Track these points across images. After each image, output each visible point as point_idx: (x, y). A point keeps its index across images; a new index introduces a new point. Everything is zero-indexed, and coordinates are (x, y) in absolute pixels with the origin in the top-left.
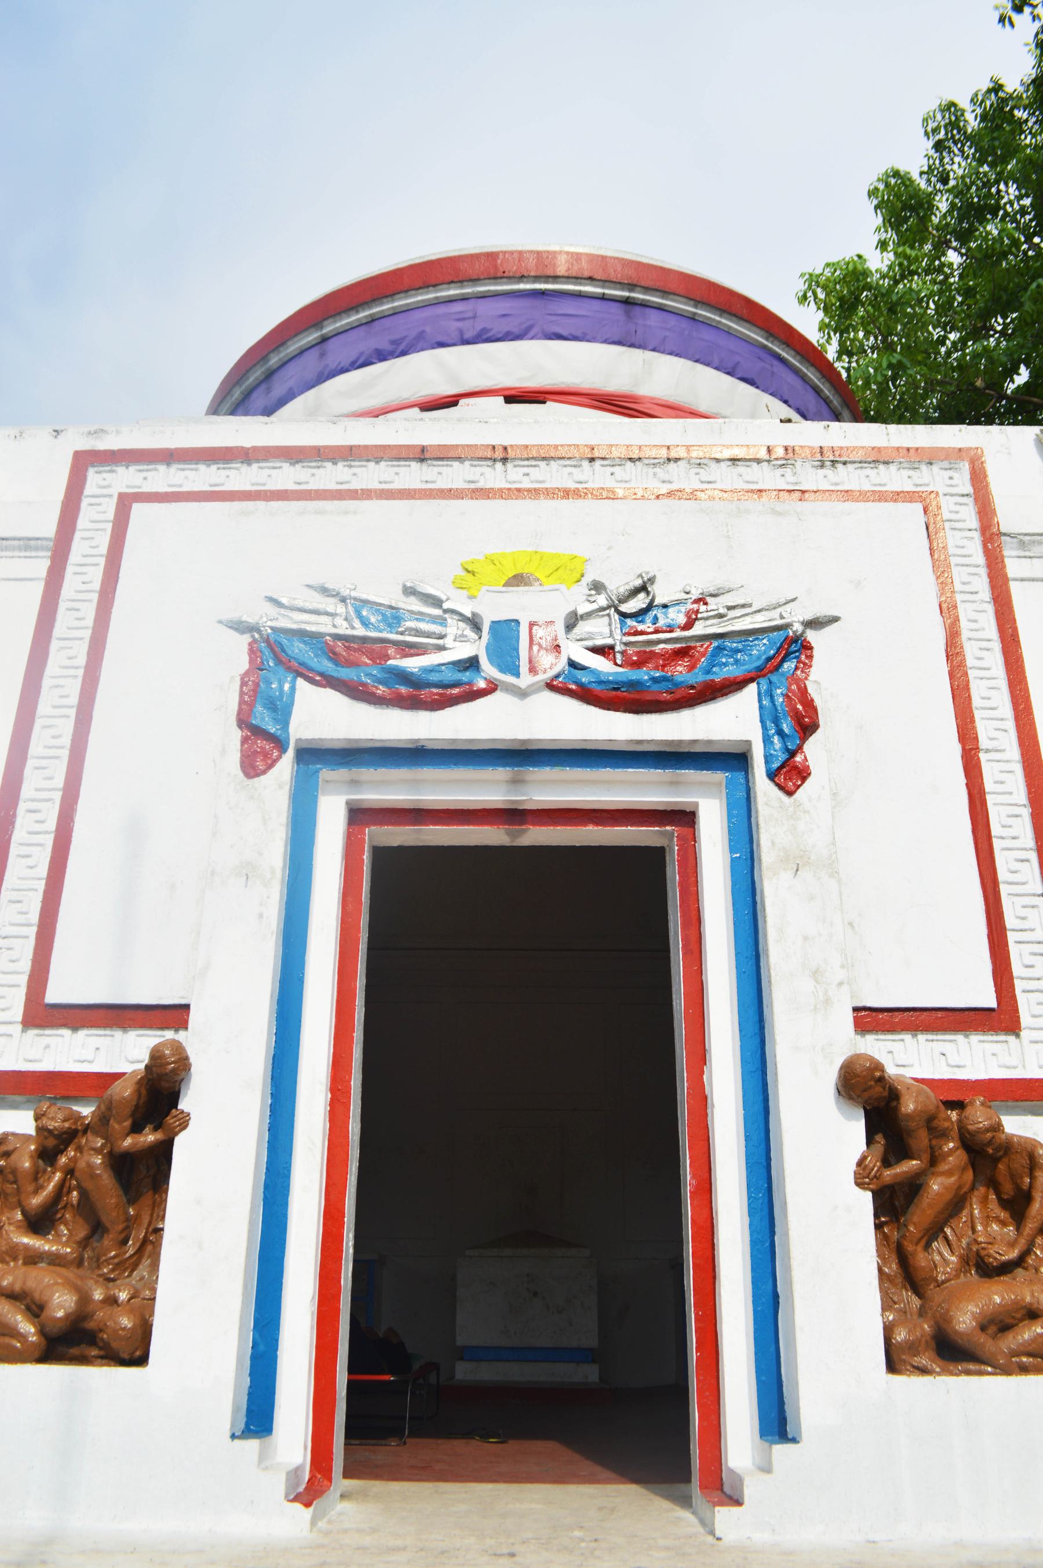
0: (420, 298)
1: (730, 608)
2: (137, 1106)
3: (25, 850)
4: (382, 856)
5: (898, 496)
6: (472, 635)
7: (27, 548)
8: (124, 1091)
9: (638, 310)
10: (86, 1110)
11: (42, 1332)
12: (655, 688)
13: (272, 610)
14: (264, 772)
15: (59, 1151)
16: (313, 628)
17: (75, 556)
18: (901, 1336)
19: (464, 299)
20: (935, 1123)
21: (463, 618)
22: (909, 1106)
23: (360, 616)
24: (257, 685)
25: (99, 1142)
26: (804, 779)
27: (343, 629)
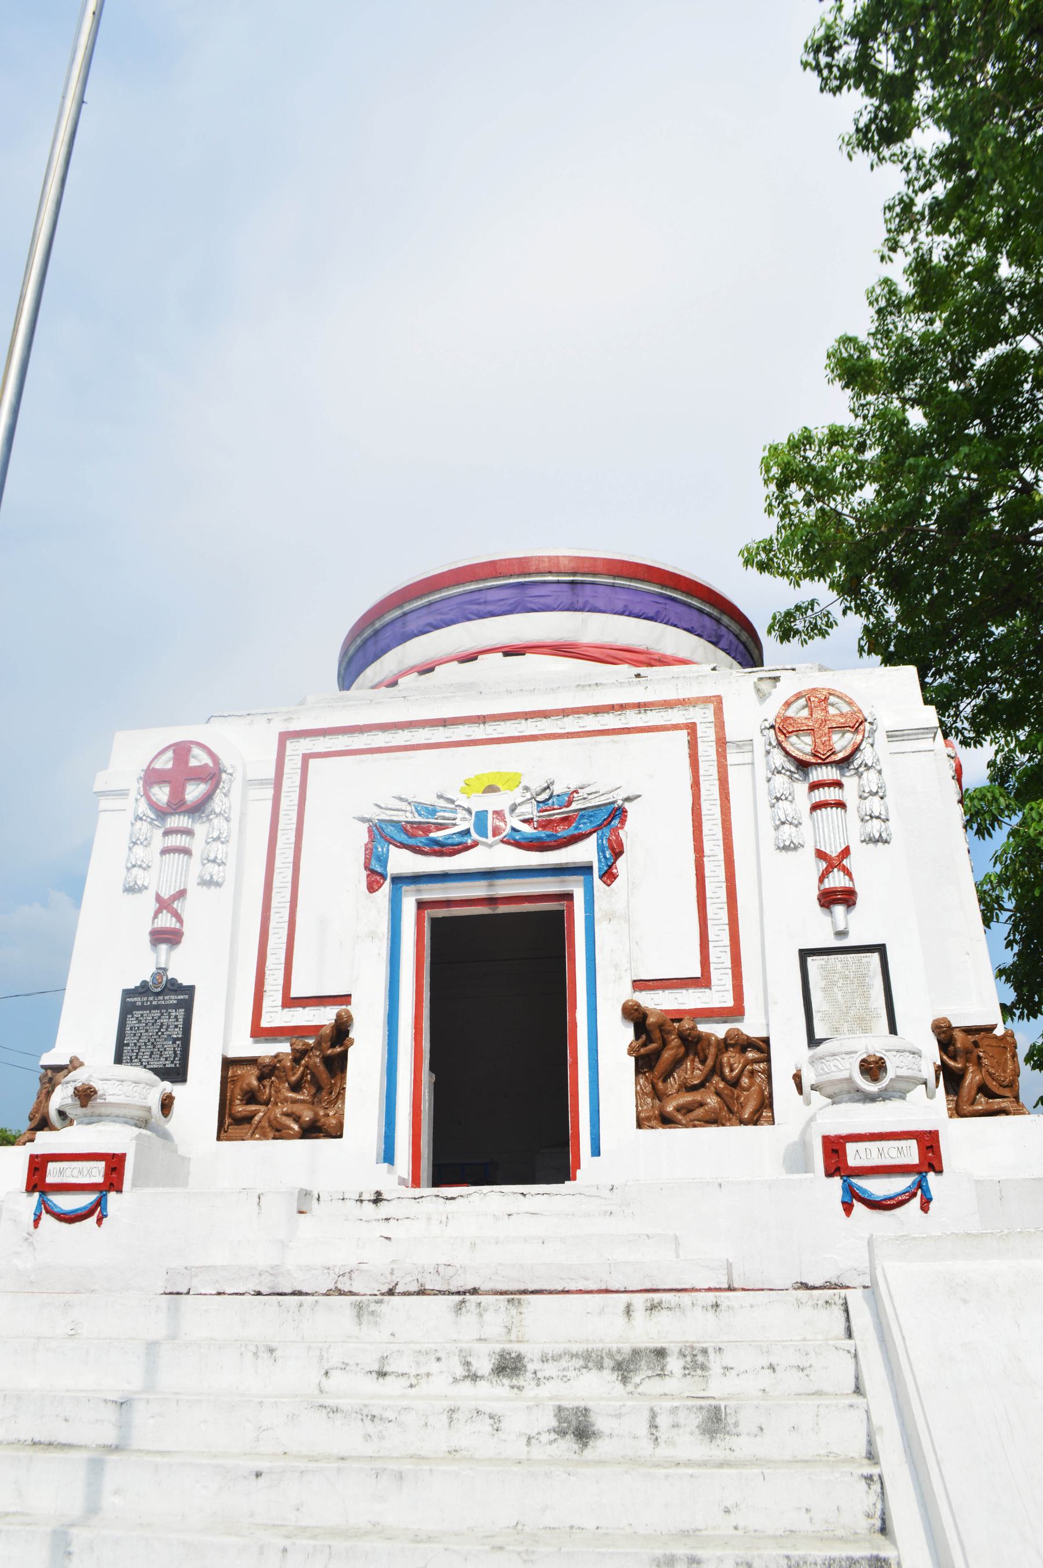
1: (589, 794)
4: (434, 921)
5: (676, 727)
6: (467, 816)
7: (262, 784)
8: (327, 1031)
9: (579, 586)
11: (300, 1127)
12: (549, 839)
13: (378, 810)
14: (377, 890)
15: (302, 1058)
16: (395, 818)
18: (642, 1115)
19: (480, 590)
20: (663, 1028)
22: (651, 1020)
23: (417, 811)
26: (615, 878)
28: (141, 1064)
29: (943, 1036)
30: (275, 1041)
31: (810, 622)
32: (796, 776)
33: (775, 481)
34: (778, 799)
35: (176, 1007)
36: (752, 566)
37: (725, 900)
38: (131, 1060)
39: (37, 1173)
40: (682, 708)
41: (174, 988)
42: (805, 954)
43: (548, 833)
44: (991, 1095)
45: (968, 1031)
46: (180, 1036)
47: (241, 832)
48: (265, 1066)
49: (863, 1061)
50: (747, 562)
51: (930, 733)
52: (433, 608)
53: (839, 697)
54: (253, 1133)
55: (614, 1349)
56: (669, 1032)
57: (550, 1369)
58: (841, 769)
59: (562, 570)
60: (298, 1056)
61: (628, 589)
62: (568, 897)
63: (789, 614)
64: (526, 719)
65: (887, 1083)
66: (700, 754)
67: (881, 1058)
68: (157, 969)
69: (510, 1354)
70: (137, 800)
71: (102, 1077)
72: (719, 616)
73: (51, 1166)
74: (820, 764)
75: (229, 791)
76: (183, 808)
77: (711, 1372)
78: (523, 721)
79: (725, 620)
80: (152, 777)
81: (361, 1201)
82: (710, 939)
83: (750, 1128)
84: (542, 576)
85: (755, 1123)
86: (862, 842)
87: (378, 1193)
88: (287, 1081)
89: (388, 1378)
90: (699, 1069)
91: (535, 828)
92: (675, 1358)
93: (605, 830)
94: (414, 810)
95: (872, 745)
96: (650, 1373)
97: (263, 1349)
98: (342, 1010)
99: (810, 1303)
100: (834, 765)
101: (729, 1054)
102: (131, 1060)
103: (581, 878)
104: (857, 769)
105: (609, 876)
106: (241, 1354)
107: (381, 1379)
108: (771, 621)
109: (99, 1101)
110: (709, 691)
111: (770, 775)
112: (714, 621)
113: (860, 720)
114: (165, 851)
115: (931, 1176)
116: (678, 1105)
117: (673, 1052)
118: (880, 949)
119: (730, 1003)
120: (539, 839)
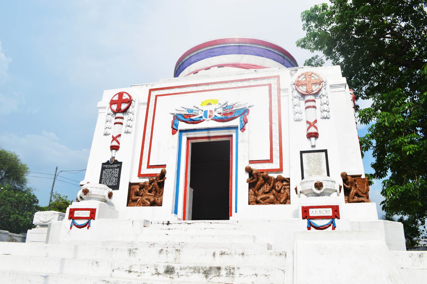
0: (204, 49)
1: (238, 105)
2: (160, 177)
3: (146, 146)
4: (193, 144)
7: (144, 104)
10: (155, 178)
11: (150, 203)
12: (225, 119)
13: (176, 111)
14: (175, 134)
17: (150, 105)
19: (212, 49)
21: (201, 110)
22: (254, 172)
23: (188, 111)
24: (174, 122)
25: (156, 181)
26: (245, 130)
27: (186, 113)
28: (106, 184)
29: (344, 178)
30: (145, 178)
31: (316, 62)
32: (301, 99)
33: (305, 20)
34: (295, 106)
35: (117, 168)
36: (299, 47)
37: (278, 137)
38: (104, 183)
39: (71, 214)
40: (267, 79)
41: (116, 163)
42: (302, 153)
43: (225, 116)
44: (359, 196)
45: (353, 176)
46: (118, 176)
47: (137, 118)
48: (141, 185)
49: (316, 183)
50: (298, 45)
51: (344, 85)
52: (198, 54)
53: (315, 74)
54: (137, 204)
55: (204, 267)
56: (260, 176)
57: (183, 272)
58: (315, 96)
59: (236, 42)
60: (151, 182)
61: (256, 47)
62: (231, 136)
63: (310, 60)
64: (221, 84)
65: (323, 190)
66: (272, 93)
67: (321, 183)
68: (112, 157)
69: (170, 267)
70: (108, 109)
71: (91, 187)
72: (284, 56)
73: (76, 212)
74: (308, 95)
75: (134, 106)
76: (120, 111)
77: (235, 276)
78: (220, 84)
79: (286, 57)
80: (112, 102)
81: (164, 224)
82: (273, 148)
83: (283, 205)
84: (230, 44)
85: (285, 204)
86: (321, 118)
87: (169, 222)
88: (147, 190)
89: (132, 273)
90: (268, 187)
91: (222, 116)
92: (224, 270)
93: (242, 116)
94: (187, 111)
95: (325, 89)
96: (215, 275)
97: (95, 262)
98: (163, 169)
99: (274, 254)
100: (313, 95)
101: (278, 183)
102: (104, 183)
103: (235, 130)
104: (320, 96)
105: (243, 129)
106: (88, 263)
107: (129, 273)
108: (305, 62)
109: (90, 193)
110: (276, 74)
111: (293, 99)
112: (282, 58)
113: (321, 81)
114: (115, 124)
115: (336, 220)
116: (261, 198)
117: (260, 182)
118: (326, 151)
119: (279, 167)
120: (222, 118)
